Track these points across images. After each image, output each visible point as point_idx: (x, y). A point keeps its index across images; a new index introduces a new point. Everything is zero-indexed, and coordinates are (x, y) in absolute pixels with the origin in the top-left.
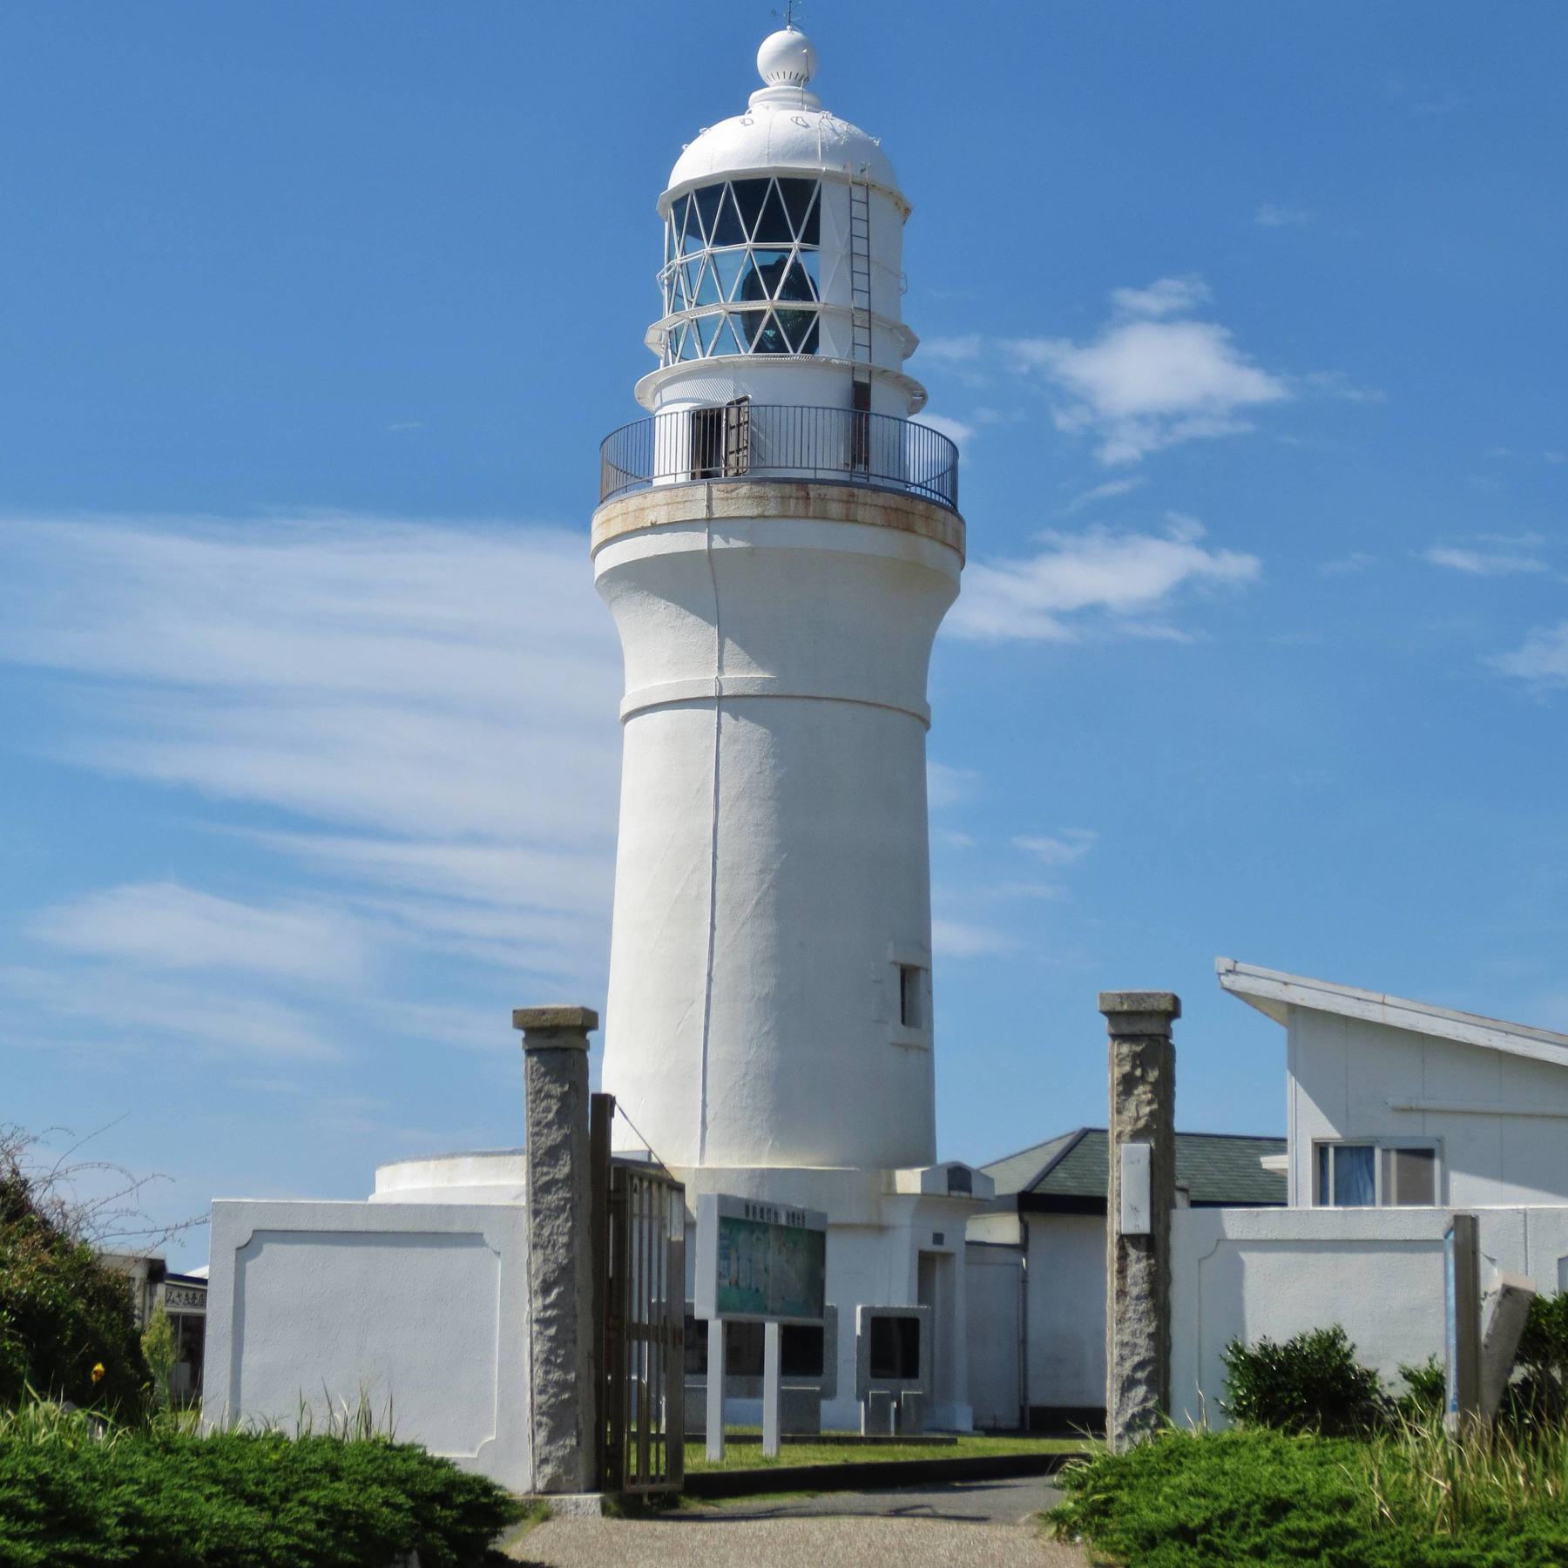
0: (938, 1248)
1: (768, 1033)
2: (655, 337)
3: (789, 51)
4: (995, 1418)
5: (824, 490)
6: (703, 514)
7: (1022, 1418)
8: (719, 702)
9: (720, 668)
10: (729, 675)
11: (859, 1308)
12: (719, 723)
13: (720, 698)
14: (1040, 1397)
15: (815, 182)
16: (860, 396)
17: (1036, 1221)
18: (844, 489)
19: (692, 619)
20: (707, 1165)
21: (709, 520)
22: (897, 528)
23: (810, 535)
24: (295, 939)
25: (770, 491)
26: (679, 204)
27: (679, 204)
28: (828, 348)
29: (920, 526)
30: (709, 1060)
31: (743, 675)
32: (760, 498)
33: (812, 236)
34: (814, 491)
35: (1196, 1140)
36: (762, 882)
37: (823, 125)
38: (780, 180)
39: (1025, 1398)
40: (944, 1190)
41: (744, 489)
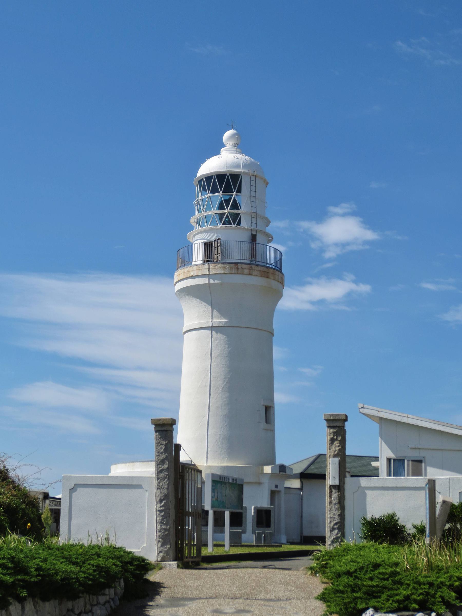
0: (276, 489)
1: (226, 426)
2: (193, 221)
3: (232, 136)
5: (243, 266)
6: (207, 273)
8: (212, 328)
9: (212, 318)
10: (215, 320)
11: (253, 507)
12: (212, 335)
13: (212, 327)
16: (253, 238)
17: (305, 481)
18: (249, 266)
20: (208, 465)
21: (209, 274)
23: (238, 279)
24: (88, 398)
25: (227, 266)
27: (200, 182)
28: (244, 224)
30: (209, 434)
31: (219, 320)
33: (239, 191)
34: (240, 266)
35: (352, 457)
36: (224, 381)
39: (302, 534)
40: (278, 472)
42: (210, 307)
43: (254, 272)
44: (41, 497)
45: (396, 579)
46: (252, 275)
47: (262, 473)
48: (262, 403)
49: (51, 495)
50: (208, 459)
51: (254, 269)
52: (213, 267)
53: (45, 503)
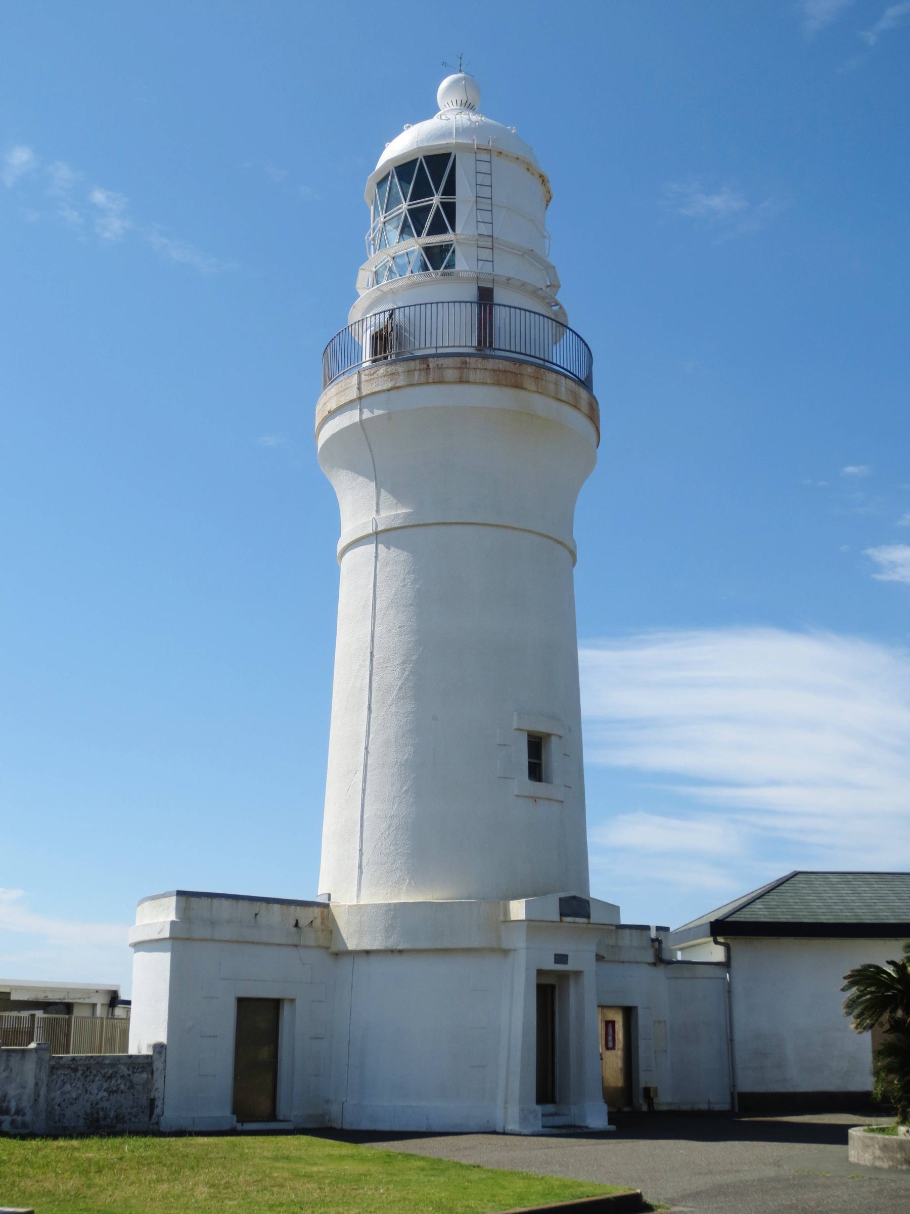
0: (561, 967)
1: (407, 791)
3: (455, 83)
4: (709, 1103)
7: (732, 1103)
9: (377, 511)
10: (383, 514)
12: (376, 553)
13: (377, 533)
14: (747, 1084)
16: (485, 297)
17: (740, 946)
18: (458, 359)
19: (361, 479)
20: (362, 903)
21: (360, 398)
22: (507, 386)
23: (431, 396)
28: (462, 264)
29: (529, 384)
30: (365, 816)
33: (450, 190)
34: (432, 363)
35: (889, 877)
36: (404, 670)
37: (466, 118)
38: (425, 157)
39: (734, 1086)
40: (556, 917)
41: (382, 370)
42: (373, 485)
43: (472, 376)
44: (101, 1001)
46: (468, 382)
47: (507, 921)
50: (363, 888)
51: (473, 365)
52: (368, 378)
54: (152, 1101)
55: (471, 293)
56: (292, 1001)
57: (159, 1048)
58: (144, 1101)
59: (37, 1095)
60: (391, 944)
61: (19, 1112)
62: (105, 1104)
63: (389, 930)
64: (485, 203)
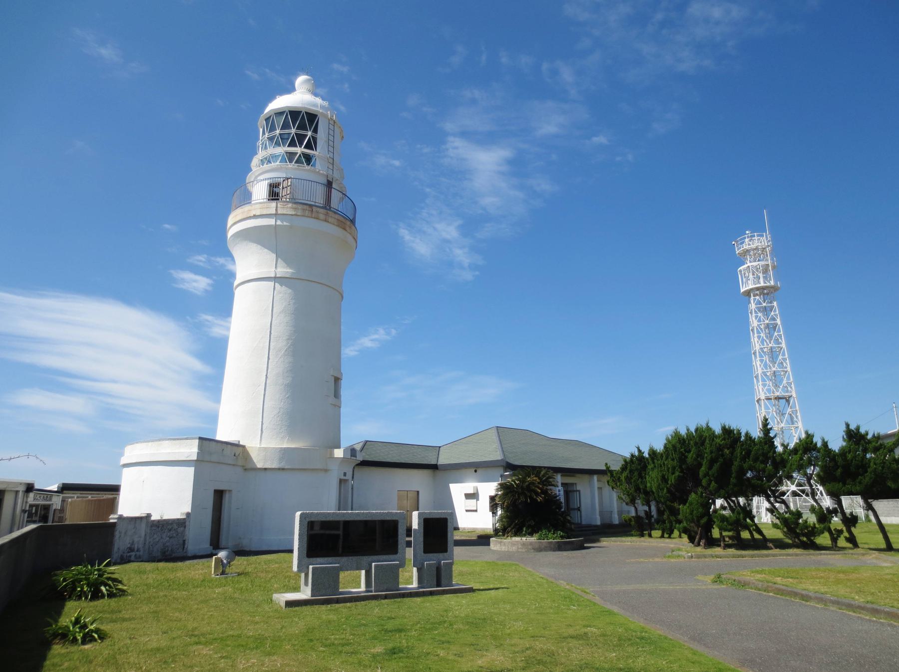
2: (255, 161)
3: (307, 81)
5: (318, 209)
6: (274, 212)
8: (275, 279)
11: (298, 514)
13: (275, 277)
15: (316, 116)
21: (276, 214)
24: (75, 404)
25: (300, 207)
26: (267, 120)
27: (267, 120)
31: (283, 270)
32: (295, 209)
33: (315, 131)
34: (315, 209)
43: (330, 220)
44: (22, 489)
45: (655, 516)
47: (331, 457)
48: (332, 373)
49: (37, 487)
53: (27, 497)
54: (184, 541)
55: (324, 181)
56: (230, 491)
57: (188, 514)
58: (181, 542)
59: (145, 540)
60: (281, 465)
61: (138, 550)
62: (168, 544)
63: (281, 460)
64: (331, 145)
